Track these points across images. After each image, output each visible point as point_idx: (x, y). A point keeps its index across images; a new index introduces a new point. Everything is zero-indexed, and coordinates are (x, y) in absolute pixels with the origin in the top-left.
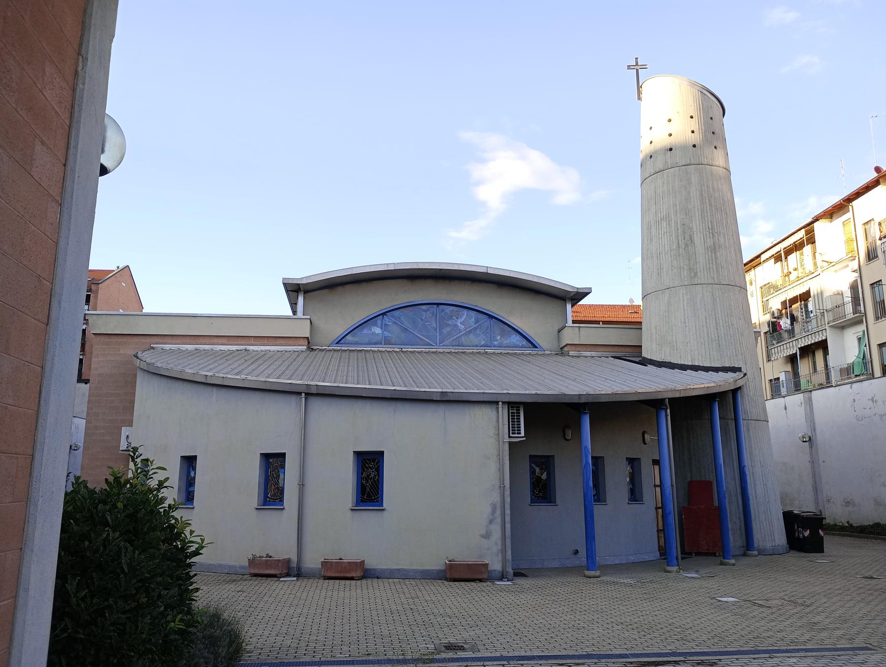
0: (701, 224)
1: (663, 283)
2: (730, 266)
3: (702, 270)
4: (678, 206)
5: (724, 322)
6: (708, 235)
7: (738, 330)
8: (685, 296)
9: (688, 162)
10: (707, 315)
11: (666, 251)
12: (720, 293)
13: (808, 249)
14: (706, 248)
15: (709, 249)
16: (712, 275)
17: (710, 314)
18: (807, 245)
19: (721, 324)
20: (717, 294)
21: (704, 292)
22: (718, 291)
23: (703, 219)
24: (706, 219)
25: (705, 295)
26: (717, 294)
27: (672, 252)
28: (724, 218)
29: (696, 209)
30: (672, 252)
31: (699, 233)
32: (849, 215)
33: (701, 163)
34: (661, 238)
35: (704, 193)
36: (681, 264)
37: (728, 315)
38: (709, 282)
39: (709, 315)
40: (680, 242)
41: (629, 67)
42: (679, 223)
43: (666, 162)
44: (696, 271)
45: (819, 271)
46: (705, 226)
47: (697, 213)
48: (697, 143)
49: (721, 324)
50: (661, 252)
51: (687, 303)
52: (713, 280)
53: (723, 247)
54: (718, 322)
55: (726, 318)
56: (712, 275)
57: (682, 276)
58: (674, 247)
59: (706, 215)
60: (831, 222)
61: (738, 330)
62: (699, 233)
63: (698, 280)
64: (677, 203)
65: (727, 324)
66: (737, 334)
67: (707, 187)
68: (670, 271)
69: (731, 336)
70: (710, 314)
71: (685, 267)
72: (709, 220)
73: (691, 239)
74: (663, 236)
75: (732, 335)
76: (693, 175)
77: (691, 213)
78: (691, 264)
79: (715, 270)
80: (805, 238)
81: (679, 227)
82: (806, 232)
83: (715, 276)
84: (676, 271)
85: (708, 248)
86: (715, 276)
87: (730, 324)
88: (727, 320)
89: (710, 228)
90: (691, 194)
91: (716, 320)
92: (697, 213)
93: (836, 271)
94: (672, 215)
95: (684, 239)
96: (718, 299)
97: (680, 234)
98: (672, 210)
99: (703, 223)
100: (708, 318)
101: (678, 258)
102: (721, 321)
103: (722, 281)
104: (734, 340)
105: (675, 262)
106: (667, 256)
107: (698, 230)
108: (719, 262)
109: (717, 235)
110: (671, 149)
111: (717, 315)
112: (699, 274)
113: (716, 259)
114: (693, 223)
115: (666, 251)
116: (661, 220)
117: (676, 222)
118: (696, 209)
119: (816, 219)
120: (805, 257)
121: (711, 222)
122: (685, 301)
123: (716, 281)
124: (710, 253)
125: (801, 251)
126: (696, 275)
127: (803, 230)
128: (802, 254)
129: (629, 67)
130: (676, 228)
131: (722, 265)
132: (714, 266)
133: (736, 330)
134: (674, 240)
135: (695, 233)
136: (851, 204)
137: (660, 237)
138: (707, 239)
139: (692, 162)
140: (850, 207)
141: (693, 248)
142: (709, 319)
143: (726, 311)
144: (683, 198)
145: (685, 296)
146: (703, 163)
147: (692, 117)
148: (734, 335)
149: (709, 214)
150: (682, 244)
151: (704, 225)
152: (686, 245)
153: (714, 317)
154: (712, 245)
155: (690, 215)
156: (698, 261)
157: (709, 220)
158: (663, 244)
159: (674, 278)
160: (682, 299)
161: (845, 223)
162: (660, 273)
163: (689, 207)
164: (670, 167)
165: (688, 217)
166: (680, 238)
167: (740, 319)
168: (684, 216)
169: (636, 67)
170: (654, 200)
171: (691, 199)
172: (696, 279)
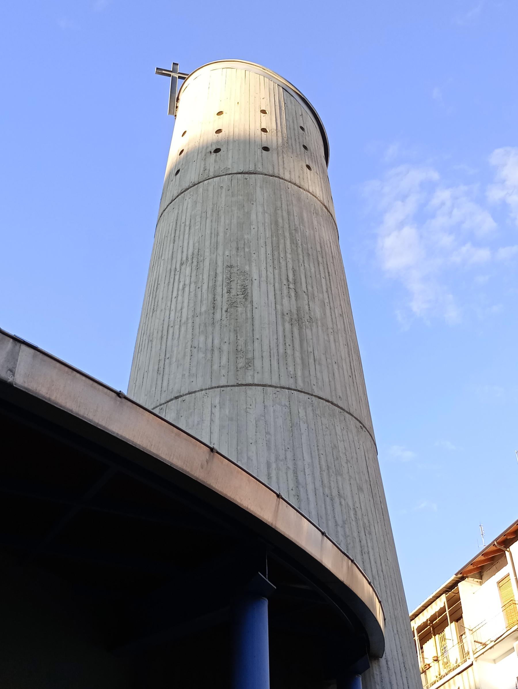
0: (270, 269)
1: (164, 388)
2: (335, 366)
3: (266, 354)
4: (221, 234)
5: (318, 484)
6: (285, 291)
7: (356, 514)
8: (217, 411)
9: (252, 168)
10: (273, 459)
11: (184, 319)
12: (311, 415)
13: (451, 630)
14: (279, 313)
15: (287, 318)
16: (291, 369)
17: (282, 457)
18: (451, 623)
19: (310, 487)
20: (302, 413)
21: (269, 403)
22: (305, 408)
23: (276, 262)
24: (283, 263)
25: (271, 409)
26: (302, 413)
27: (197, 320)
28: (323, 275)
29: (262, 241)
30: (197, 320)
31: (264, 285)
32: (507, 569)
33: (276, 175)
34: (177, 297)
35: (280, 221)
36: (217, 342)
37: (328, 468)
38: (283, 383)
39: (277, 459)
40: (219, 298)
41: (160, 71)
42: (220, 263)
43: (205, 170)
44: (250, 356)
45: (472, 657)
46: (280, 275)
47: (263, 250)
48: (273, 145)
49: (310, 487)
50: (172, 324)
51: (222, 427)
52: (292, 381)
53: (319, 323)
54: (301, 479)
55: (325, 474)
56: (291, 369)
57: (216, 367)
58: (204, 309)
59: (282, 255)
60: (481, 584)
61: (356, 514)
62: (264, 285)
63: (253, 376)
64: (221, 230)
65: (327, 491)
66: (354, 523)
67: (289, 213)
68: (188, 358)
69: (337, 525)
70: (282, 457)
71: (225, 347)
72: (290, 266)
73: (245, 292)
74: (180, 292)
75: (340, 522)
76: (258, 189)
77: (249, 247)
78: (241, 342)
79: (298, 361)
80: (447, 612)
81: (219, 270)
82: (448, 600)
83: (299, 373)
84: (201, 355)
85: (283, 315)
86: (299, 373)
87: (335, 492)
88: (326, 481)
89: (291, 279)
90: (253, 217)
91: (295, 472)
92: (263, 250)
93: (494, 660)
94: (207, 250)
95: (229, 292)
96: (303, 426)
97: (219, 283)
98: (207, 243)
99: (274, 268)
100: (274, 466)
101: (210, 329)
102: (309, 479)
103: (314, 388)
104: (346, 536)
105: (202, 339)
106: (183, 329)
107: (264, 278)
108: (310, 349)
109: (306, 297)
110: (217, 151)
111: (300, 463)
112: (258, 363)
113: (301, 341)
114: (254, 264)
115: (184, 319)
116: (182, 264)
117: (214, 264)
118: (262, 241)
119: (462, 576)
120: (448, 644)
121: (294, 271)
122: (217, 421)
123: (300, 385)
124: (287, 326)
125: (441, 635)
126: (249, 363)
127: (443, 598)
128: (444, 639)
129: (160, 71)
130: (212, 273)
131: (317, 357)
132: (298, 354)
133: (352, 513)
134: (205, 296)
135: (256, 283)
136: (508, 549)
137: (175, 294)
138: (282, 298)
139: (260, 169)
140: (507, 554)
141: (249, 308)
142: (278, 469)
143: (323, 458)
144: (235, 221)
145: (217, 411)
146: (282, 175)
147: (264, 112)
148: (344, 522)
149: (289, 256)
150: (222, 302)
151: (276, 272)
152: (232, 304)
153: (290, 465)
154: (294, 311)
155: (247, 250)
156: (257, 336)
157: (290, 266)
158: (179, 308)
159: (193, 371)
160: (207, 419)
161: (501, 584)
162: (161, 369)
163: (246, 236)
164: (211, 175)
165: (242, 254)
166: (219, 290)
167: (360, 489)
168: (234, 252)
169: (172, 74)
170: (173, 236)
171: (251, 224)
172: (250, 373)
